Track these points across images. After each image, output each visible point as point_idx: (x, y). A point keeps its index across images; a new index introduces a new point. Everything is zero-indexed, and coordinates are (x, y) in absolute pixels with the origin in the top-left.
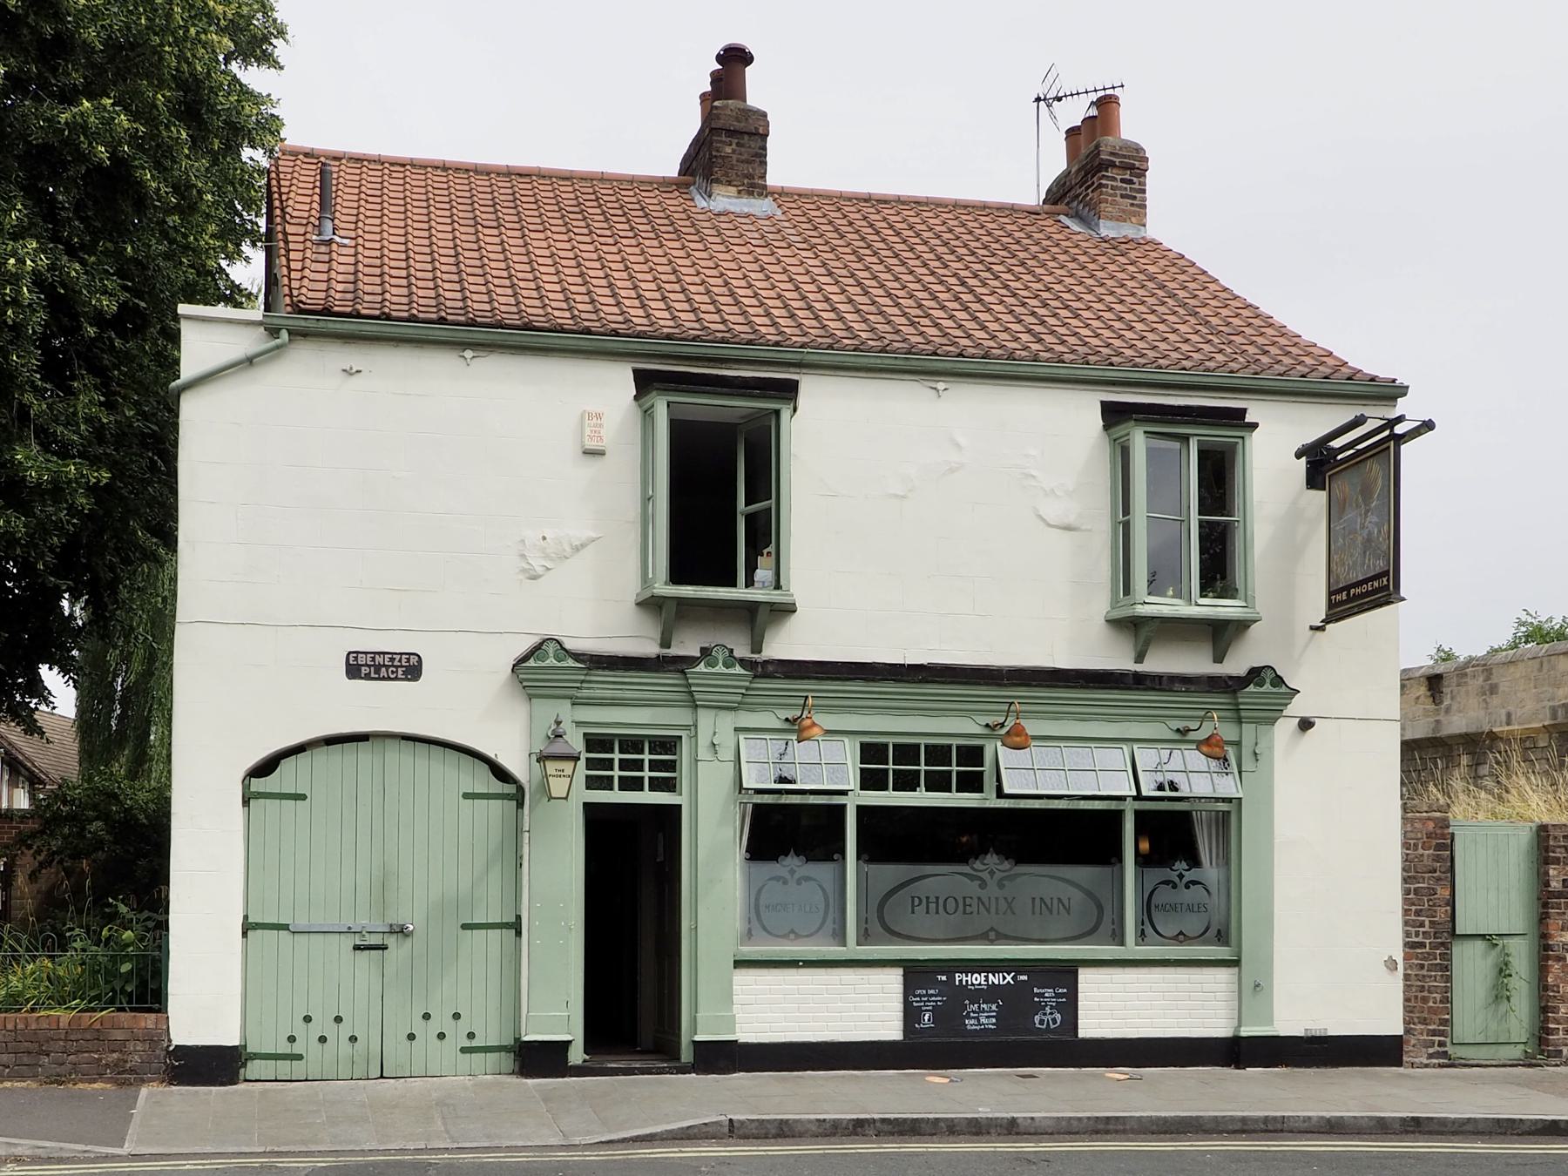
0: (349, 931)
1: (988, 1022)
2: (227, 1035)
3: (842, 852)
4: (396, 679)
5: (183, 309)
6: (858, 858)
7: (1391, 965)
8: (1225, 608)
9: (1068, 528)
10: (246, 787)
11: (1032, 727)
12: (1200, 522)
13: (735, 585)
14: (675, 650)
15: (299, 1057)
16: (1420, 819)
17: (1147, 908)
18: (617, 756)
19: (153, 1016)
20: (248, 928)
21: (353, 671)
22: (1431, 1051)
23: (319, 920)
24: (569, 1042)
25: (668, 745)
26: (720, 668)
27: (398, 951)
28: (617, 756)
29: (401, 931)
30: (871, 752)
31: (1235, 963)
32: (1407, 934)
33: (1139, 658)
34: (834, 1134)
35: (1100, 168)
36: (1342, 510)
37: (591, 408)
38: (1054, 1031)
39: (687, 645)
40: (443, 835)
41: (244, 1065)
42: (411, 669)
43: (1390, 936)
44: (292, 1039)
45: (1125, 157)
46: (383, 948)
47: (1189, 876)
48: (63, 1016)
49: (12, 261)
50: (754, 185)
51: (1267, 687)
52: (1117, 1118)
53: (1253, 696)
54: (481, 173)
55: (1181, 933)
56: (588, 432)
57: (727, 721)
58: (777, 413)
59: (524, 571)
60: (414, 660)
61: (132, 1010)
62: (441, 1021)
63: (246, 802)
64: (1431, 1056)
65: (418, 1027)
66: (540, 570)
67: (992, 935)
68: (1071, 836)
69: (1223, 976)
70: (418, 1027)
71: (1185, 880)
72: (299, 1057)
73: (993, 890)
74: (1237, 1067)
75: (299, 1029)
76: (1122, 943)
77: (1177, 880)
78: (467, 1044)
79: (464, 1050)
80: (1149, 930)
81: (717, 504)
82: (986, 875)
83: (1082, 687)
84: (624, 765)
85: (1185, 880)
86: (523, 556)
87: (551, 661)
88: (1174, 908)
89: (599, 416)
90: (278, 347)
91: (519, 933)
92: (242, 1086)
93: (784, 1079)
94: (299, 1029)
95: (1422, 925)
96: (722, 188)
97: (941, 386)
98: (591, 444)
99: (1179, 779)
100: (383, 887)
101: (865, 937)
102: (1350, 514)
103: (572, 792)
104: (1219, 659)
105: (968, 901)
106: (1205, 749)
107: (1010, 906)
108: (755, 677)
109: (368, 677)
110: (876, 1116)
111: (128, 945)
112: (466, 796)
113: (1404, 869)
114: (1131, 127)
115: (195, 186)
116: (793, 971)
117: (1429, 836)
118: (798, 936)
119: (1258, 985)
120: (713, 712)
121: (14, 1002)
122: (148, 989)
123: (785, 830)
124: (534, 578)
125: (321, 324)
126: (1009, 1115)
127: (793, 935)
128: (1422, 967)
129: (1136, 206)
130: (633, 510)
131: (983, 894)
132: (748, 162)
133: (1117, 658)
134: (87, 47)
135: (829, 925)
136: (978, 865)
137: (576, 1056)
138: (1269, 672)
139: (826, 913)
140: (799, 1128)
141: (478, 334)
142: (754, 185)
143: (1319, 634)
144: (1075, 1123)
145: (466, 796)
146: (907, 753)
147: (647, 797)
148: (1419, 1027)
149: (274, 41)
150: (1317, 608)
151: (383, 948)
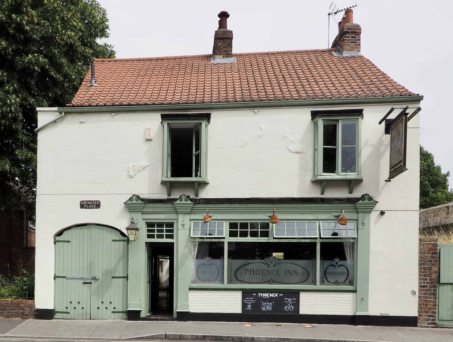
0: (82, 278)
1: (269, 308)
2: (50, 307)
3: (223, 256)
4: (93, 208)
5: (38, 109)
6: (228, 258)
7: (414, 293)
8: (351, 176)
9: (298, 153)
10: (55, 239)
11: (280, 216)
12: (324, 149)
13: (192, 177)
14: (172, 197)
15: (69, 313)
16: (426, 244)
17: (325, 274)
18: (156, 228)
19: (31, 301)
20: (55, 277)
21: (82, 206)
22: (429, 322)
23: (74, 275)
24: (141, 311)
25: (171, 225)
26: (184, 202)
27: (95, 284)
28: (156, 228)
29: (95, 279)
30: (233, 225)
31: (355, 291)
32: (420, 283)
33: (322, 193)
34: (196, 340)
35: (348, 34)
36: (394, 141)
37: (148, 127)
38: (291, 312)
39: (175, 195)
40: (107, 252)
41: (55, 314)
42: (97, 205)
43: (414, 284)
44: (67, 308)
45: (353, 29)
46: (91, 283)
47: (340, 263)
48: (9, 299)
49: (8, 101)
50: (228, 54)
51: (366, 201)
52: (287, 339)
53: (362, 205)
54: (150, 60)
55: (336, 281)
56: (147, 134)
57: (188, 217)
58: (201, 123)
59: (129, 176)
60: (98, 203)
61: (28, 299)
62: (106, 304)
63: (55, 243)
64: (428, 324)
65: (100, 305)
66: (133, 175)
67: (271, 282)
68: (298, 251)
69: (350, 296)
70: (100, 305)
71: (338, 265)
72: (69, 313)
73: (272, 267)
74: (355, 325)
75: (69, 305)
76: (316, 285)
77: (335, 264)
78: (114, 310)
79: (113, 312)
80: (325, 280)
81: (184, 154)
82: (269, 263)
83: (301, 203)
84: (158, 231)
85: (338, 265)
86: (128, 171)
87: (134, 201)
88: (334, 273)
89: (150, 129)
90: (61, 117)
91: (128, 280)
92: (53, 320)
93: (202, 323)
94: (69, 305)
95: (426, 279)
96: (218, 56)
97: (256, 111)
98: (148, 137)
99: (339, 232)
100: (91, 266)
101: (230, 282)
102: (395, 142)
103: (142, 238)
104: (351, 192)
105: (264, 271)
106: (340, 222)
107: (277, 273)
108: (194, 204)
109: (86, 208)
110: (210, 335)
111: (26, 282)
112: (113, 241)
113: (419, 261)
114: (356, 19)
115: (69, 74)
116: (208, 291)
117: (430, 249)
118: (209, 281)
119: (363, 299)
120: (183, 215)
121: (2, 296)
122: (30, 294)
123: (210, 250)
124: (131, 177)
125: (72, 110)
126: (252, 336)
127: (209, 281)
128: (426, 294)
129: (357, 44)
130: (160, 157)
131: (269, 269)
132: (226, 47)
133: (315, 193)
134: (36, 40)
135: (219, 278)
136: (267, 260)
137: (143, 315)
138: (367, 196)
139: (218, 274)
140: (186, 337)
141: (115, 108)
142: (228, 54)
143: (388, 183)
144: (273, 340)
145: (113, 241)
146: (244, 225)
147: (165, 240)
148: (424, 314)
149: (106, 30)
150: (386, 173)
151: (91, 283)
